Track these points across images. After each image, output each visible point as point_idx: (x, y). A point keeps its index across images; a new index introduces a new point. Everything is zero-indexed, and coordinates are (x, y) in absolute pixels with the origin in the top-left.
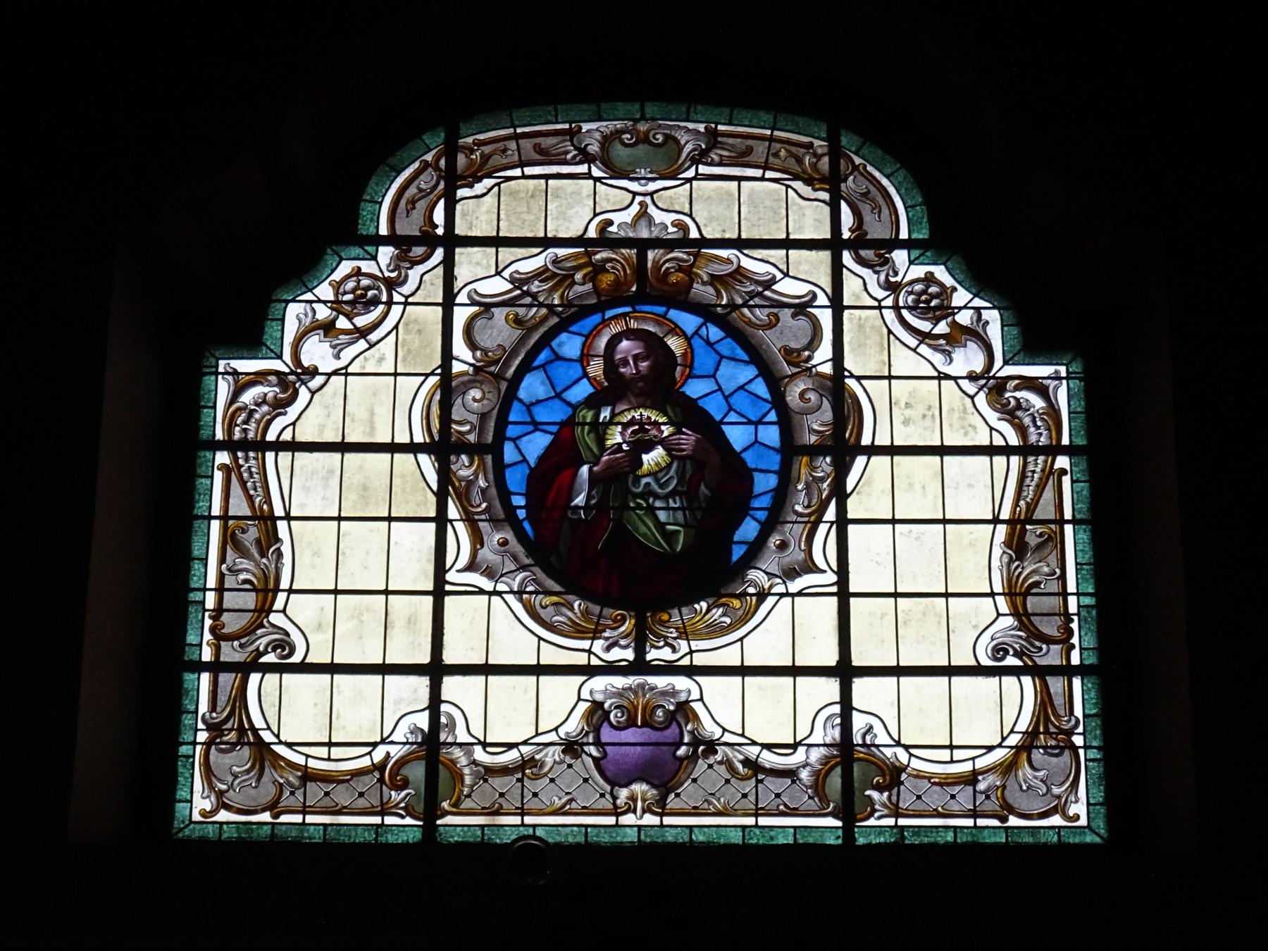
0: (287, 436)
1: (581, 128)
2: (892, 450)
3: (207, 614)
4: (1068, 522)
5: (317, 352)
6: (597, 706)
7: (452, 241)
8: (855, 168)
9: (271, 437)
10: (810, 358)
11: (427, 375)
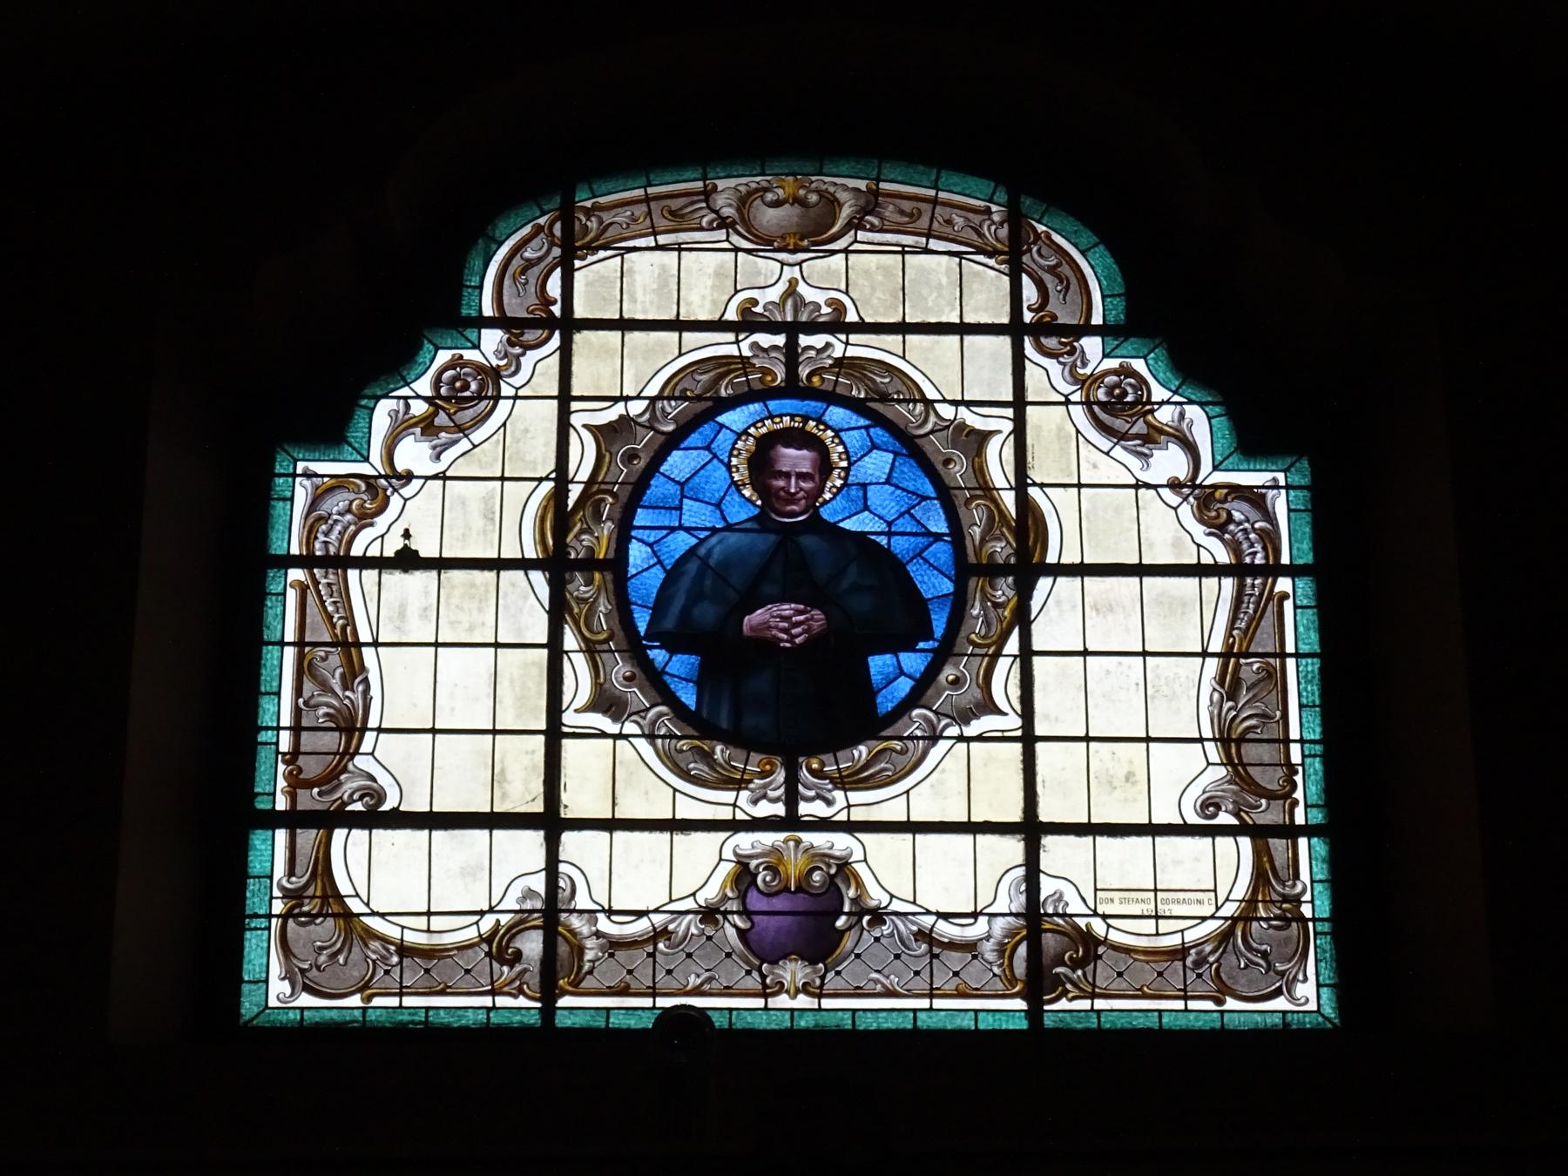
0: (374, 551)
1: (715, 187)
2: (1082, 570)
4: (1291, 655)
5: (413, 454)
6: (742, 863)
7: (569, 325)
8: (1037, 236)
9: (357, 551)
11: (540, 480)
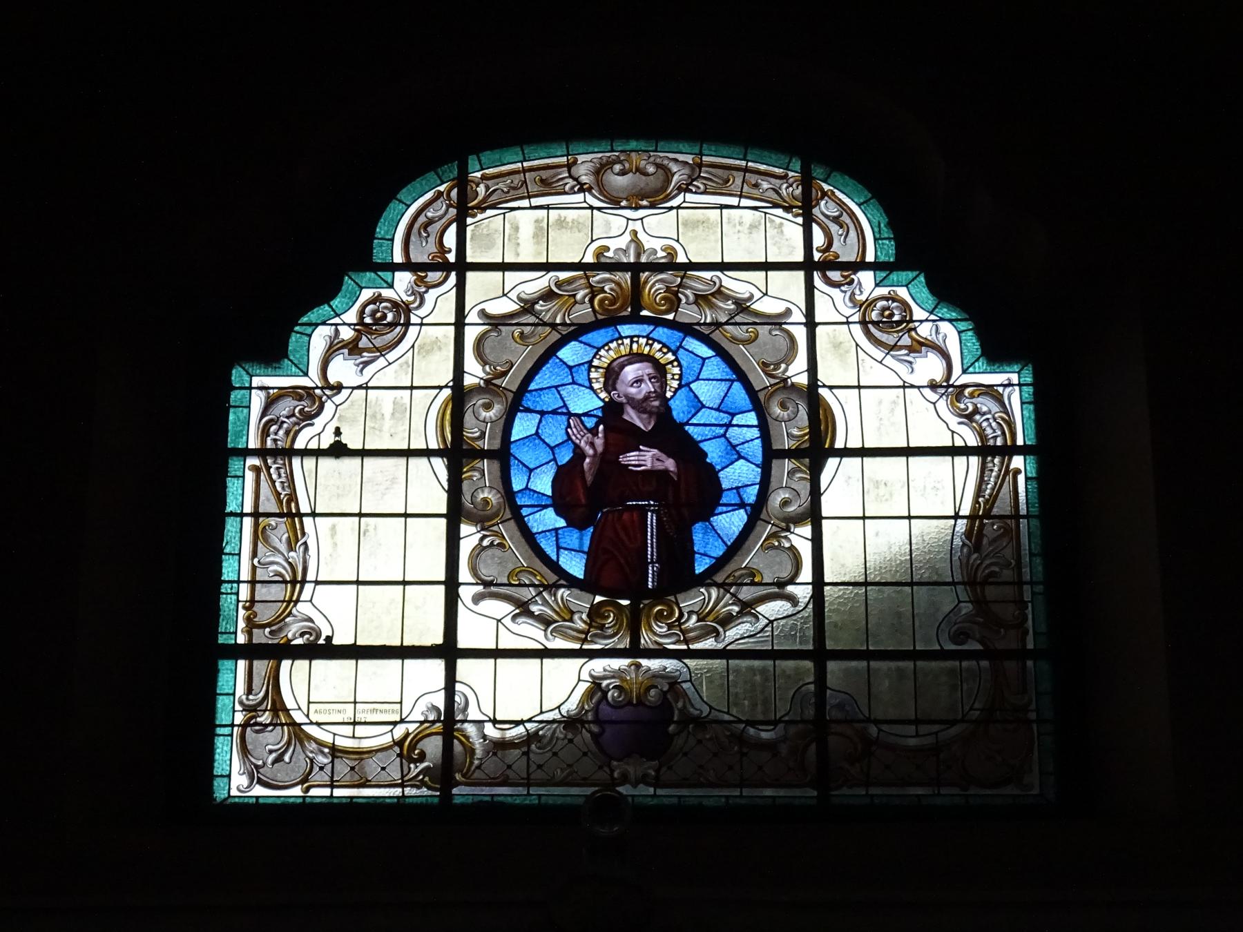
1: (576, 160)
3: (241, 605)
5: (343, 370)
8: (824, 194)
10: (786, 370)
11: (440, 388)
